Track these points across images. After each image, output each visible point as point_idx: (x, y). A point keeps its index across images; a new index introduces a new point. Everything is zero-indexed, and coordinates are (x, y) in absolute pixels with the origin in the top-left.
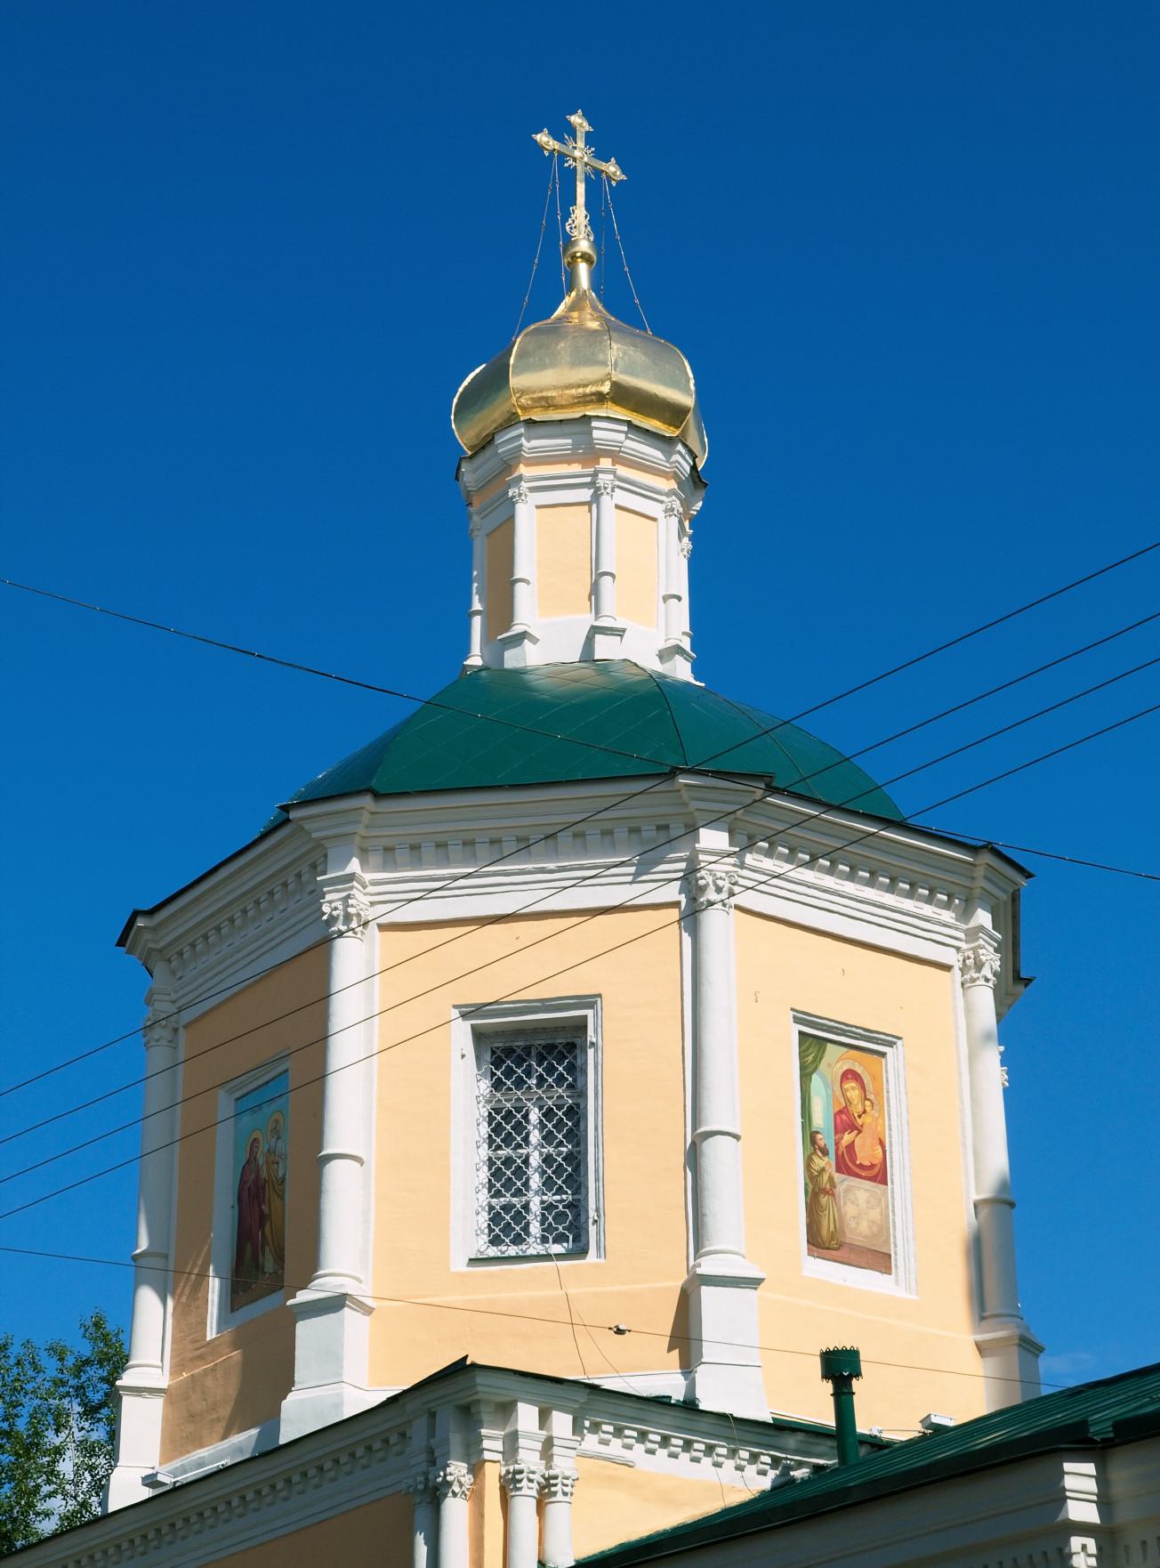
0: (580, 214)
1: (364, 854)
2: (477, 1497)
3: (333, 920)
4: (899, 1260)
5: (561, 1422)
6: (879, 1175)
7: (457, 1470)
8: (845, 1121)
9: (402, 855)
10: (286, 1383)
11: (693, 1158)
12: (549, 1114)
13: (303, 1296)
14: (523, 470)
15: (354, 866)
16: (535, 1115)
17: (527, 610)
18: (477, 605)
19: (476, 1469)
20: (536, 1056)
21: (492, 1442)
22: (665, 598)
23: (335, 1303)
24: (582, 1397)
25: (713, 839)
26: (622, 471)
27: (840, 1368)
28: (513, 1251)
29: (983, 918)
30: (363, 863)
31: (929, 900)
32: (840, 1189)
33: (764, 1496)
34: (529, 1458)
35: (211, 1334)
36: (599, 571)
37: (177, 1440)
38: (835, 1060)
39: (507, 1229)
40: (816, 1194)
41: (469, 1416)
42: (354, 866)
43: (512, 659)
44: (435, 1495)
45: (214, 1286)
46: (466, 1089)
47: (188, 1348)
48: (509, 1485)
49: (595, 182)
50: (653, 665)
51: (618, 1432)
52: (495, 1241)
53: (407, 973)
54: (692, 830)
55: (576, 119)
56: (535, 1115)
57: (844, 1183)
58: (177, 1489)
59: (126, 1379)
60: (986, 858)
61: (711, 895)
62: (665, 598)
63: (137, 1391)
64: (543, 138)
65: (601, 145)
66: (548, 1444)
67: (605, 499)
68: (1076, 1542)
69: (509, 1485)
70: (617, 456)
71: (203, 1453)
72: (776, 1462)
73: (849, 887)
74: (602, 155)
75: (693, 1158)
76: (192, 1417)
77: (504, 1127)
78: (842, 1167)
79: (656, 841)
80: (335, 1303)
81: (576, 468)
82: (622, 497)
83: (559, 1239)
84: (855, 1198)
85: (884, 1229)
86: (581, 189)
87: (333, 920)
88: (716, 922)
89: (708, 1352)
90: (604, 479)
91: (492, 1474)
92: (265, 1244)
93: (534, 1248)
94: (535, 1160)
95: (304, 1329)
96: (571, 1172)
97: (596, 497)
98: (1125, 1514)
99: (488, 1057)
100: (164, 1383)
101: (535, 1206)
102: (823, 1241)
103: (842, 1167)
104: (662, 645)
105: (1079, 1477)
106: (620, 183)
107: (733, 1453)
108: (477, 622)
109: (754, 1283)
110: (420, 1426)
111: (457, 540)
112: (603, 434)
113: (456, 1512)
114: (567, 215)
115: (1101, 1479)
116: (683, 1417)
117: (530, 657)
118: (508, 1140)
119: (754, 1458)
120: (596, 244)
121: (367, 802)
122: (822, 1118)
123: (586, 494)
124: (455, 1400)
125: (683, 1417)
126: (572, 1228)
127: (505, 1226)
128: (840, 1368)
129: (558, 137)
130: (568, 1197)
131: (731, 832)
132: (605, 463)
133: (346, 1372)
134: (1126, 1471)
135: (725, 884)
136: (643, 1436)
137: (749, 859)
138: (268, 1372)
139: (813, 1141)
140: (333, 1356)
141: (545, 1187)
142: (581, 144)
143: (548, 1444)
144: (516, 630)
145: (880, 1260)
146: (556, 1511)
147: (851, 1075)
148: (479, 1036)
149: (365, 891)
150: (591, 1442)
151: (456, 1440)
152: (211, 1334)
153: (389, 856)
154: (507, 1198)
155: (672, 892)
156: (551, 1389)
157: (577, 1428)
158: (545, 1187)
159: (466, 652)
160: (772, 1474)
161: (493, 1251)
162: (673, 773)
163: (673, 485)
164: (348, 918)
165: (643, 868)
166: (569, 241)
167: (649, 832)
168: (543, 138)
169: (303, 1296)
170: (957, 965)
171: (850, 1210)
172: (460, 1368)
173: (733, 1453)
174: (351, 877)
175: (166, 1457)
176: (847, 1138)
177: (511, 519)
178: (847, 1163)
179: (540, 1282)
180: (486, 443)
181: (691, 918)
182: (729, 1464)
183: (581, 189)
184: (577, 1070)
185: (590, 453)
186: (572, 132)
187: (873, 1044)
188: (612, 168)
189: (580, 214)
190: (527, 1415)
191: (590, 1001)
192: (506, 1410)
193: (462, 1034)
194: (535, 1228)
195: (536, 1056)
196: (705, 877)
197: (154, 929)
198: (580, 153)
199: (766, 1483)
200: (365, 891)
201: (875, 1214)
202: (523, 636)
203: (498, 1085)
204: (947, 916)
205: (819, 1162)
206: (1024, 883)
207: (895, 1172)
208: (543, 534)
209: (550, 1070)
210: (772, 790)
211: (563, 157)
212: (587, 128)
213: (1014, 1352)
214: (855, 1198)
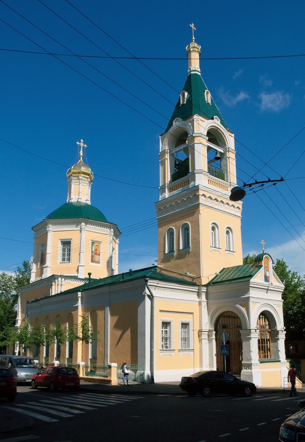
0: (81, 151)
1: (51, 224)
2: (55, 286)
3: (48, 231)
4: (100, 263)
5: (63, 279)
6: (99, 255)
7: (53, 283)
8: (96, 250)
9: (54, 224)
10: (43, 274)
11: (79, 254)
12: (68, 249)
13: (44, 266)
14: (73, 181)
15: (50, 225)
16: (66, 249)
17: (72, 197)
18: (68, 194)
19: (55, 283)
20: (66, 244)
21: (56, 281)
22: (87, 194)
23: (47, 267)
24: (65, 277)
25: (83, 224)
26: (82, 181)
27: (90, 274)
28: (64, 262)
29: (112, 230)
30: (51, 225)
31: (106, 228)
32: (95, 256)
33: (83, 285)
34: (60, 283)
35: (39, 268)
36: (81, 192)
37: (36, 277)
38: (96, 244)
39: (63, 260)
40: (92, 257)
41: (55, 279)
42: (50, 225)
43: (70, 201)
44: (52, 285)
45: (39, 263)
46: (60, 246)
47: (37, 269)
48: (58, 285)
49: (83, 147)
50: (85, 202)
51: (69, 280)
52: (62, 261)
53: (55, 235)
54: (81, 223)
55: (82, 140)
56: (66, 249)
57: (95, 256)
58: (34, 282)
59: (32, 271)
60: (112, 224)
61: (82, 229)
62: (87, 194)
63: (32, 272)
64: (78, 143)
65: (84, 143)
66: (62, 281)
67: (80, 184)
68: (79, 298)
69: (58, 285)
70: (82, 180)
71: (38, 278)
72: (85, 282)
73: (98, 228)
74: (84, 144)
75: (79, 254)
76: (37, 275)
77: (64, 250)
78: (95, 254)
79: (78, 224)
80: (47, 267)
81: (78, 181)
82: (82, 184)
83: (68, 261)
84: (96, 257)
85: (99, 260)
86: (82, 148)
87: (48, 231)
88: (83, 232)
89: (79, 272)
90: (80, 182)
91: (57, 284)
92: (42, 259)
93: (66, 262)
94: (66, 254)
95: (44, 269)
96: (69, 255)
97: (80, 184)
98: (83, 296)
99: (62, 244)
100: (35, 271)
101: (66, 258)
102: (93, 261)
103: (95, 254)
104: (86, 199)
105: (79, 294)
106: (86, 147)
107: (80, 281)
108: (68, 196)
109: (84, 266)
110: (51, 279)
111: (67, 189)
112: (80, 177)
113: (53, 287)
114: (80, 151)
115: (81, 293)
116: (76, 278)
117: (72, 201)
118: (64, 252)
119: (82, 282)
120: (83, 155)
121: (51, 219)
122: (93, 250)
123: (79, 183)
124: (53, 278)
125: (76, 278)
126: (69, 260)
127: (64, 260)
128: (90, 274)
129: (79, 142)
130: (69, 257)
131: (85, 223)
132: (81, 180)
133: (47, 274)
134: (83, 293)
135: (84, 228)
136: (71, 280)
137: (87, 225)
138: (42, 273)
139: (92, 252)
140: (47, 271)
141: (67, 256)
142: (82, 143)
143: (62, 281)
144: (71, 198)
145: (99, 263)
146: (62, 287)
147: (97, 245)
148: (61, 242)
149: (51, 229)
150: (66, 281)
151: (53, 281)
152: (39, 268)
153: (53, 224)
154: (63, 257)
155: (79, 229)
156: (62, 276)
157: (65, 280)
158: (67, 256)
159: (67, 199)
160: (84, 283)
161: (62, 262)
162: (79, 218)
163: (88, 182)
164: (49, 231)
165: (77, 227)
166: (80, 154)
167: (77, 223)
168: (78, 143)
169: (44, 266)
170: (109, 234)
171: (96, 258)
172: (53, 275)
173: (80, 281)
174: (50, 227)
175: (35, 278)
176: (96, 251)
177: (71, 186)
178: (96, 254)
179: (66, 265)
180: (69, 177)
181: (81, 232)
182: (80, 282)
183: (82, 148)
184: (70, 245)
185: (79, 179)
186: (81, 142)
187: (100, 242)
188: (86, 146)
189: (81, 151)
190: (60, 279)
191: (71, 239)
192: (58, 278)
193: (60, 242)
194: (66, 260)
195: (66, 244)
196: (82, 228)
197: (34, 229)
198: (82, 144)
199: (84, 284)
200: (51, 229)
201: (98, 258)
202: (71, 199)
203: (63, 246)
204: (108, 230)
205: (93, 254)
206: (117, 226)
207: (101, 255)
208: (74, 187)
209: (68, 245)
210: (89, 219)
211: (80, 145)
212: (83, 141)
213: (111, 271)
214: (96, 257)
